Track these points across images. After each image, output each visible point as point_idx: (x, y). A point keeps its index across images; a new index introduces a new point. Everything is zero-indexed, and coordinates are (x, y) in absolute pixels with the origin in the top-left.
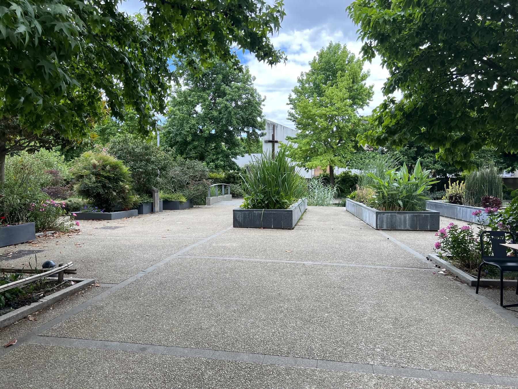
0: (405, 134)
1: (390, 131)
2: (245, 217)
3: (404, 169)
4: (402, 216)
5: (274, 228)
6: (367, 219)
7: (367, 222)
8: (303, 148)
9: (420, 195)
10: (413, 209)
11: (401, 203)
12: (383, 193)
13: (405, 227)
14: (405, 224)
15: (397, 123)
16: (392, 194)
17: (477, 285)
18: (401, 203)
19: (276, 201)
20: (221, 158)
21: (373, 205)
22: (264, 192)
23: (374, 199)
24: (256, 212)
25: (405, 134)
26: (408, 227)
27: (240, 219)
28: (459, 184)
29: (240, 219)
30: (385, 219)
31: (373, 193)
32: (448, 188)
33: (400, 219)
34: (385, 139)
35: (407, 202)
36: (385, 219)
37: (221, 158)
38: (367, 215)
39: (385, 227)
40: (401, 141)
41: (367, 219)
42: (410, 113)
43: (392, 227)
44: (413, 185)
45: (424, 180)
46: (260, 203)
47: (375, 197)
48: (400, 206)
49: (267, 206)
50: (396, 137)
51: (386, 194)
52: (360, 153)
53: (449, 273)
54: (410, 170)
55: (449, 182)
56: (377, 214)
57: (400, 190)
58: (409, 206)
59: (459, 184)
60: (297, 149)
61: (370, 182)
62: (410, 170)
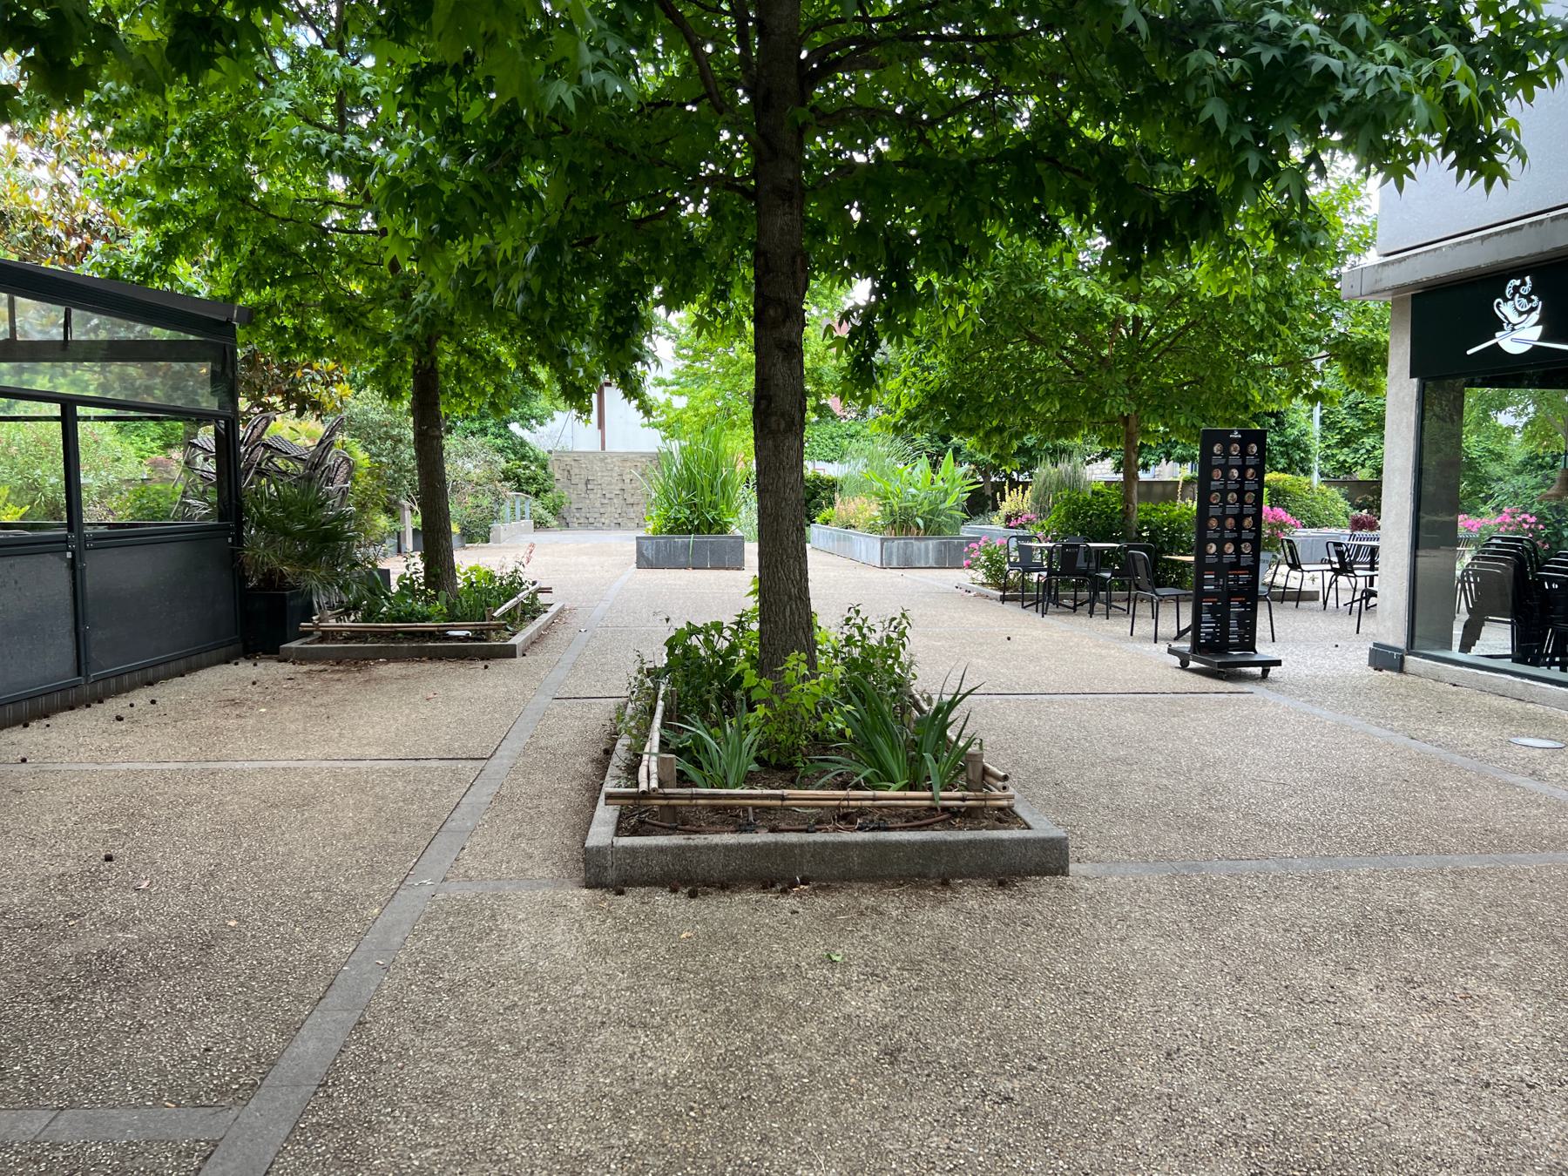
0: (928, 421)
1: (911, 416)
2: (658, 551)
3: (924, 463)
4: (923, 544)
5: (711, 568)
6: (864, 553)
7: (864, 559)
8: (703, 411)
9: (951, 508)
10: (939, 532)
11: (921, 523)
12: (892, 506)
13: (927, 562)
14: (927, 557)
15: (919, 406)
16: (906, 508)
17: (1003, 599)
18: (921, 523)
19: (713, 518)
20: (493, 429)
21: (873, 529)
22: (692, 506)
23: (874, 518)
24: (680, 540)
25: (928, 421)
26: (932, 563)
27: (650, 553)
28: (1023, 493)
29: (650, 553)
30: (895, 550)
31: (874, 506)
32: (1003, 499)
33: (919, 549)
34: (903, 426)
35: (931, 520)
36: (895, 550)
37: (493, 429)
38: (863, 547)
39: (895, 565)
40: (922, 427)
41: (864, 553)
42: (934, 395)
43: (907, 564)
44: (939, 492)
45: (958, 482)
46: (684, 523)
47: (876, 513)
48: (918, 528)
49: (697, 530)
50: (917, 423)
51: (896, 508)
52: (827, 423)
53: (979, 595)
54: (935, 466)
55: (1006, 488)
56: (883, 541)
57: (919, 500)
58: (933, 526)
59: (1023, 493)
60: (684, 411)
61: (861, 487)
62: (935, 466)
